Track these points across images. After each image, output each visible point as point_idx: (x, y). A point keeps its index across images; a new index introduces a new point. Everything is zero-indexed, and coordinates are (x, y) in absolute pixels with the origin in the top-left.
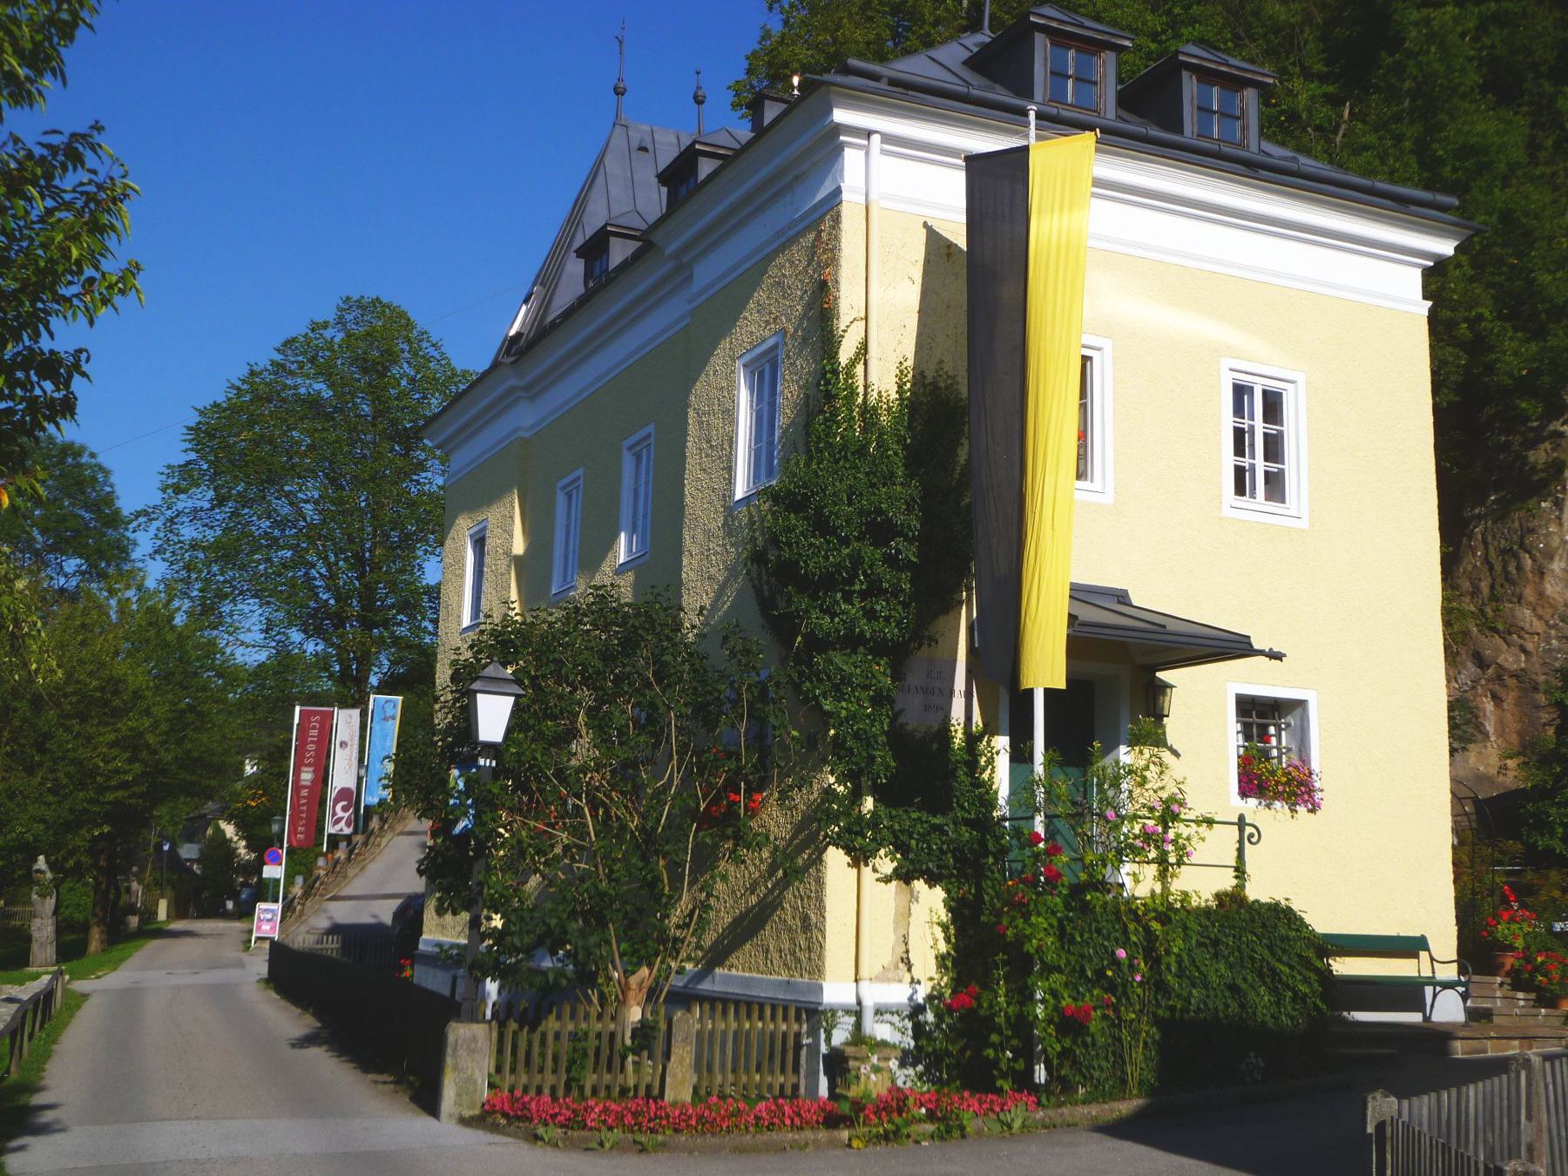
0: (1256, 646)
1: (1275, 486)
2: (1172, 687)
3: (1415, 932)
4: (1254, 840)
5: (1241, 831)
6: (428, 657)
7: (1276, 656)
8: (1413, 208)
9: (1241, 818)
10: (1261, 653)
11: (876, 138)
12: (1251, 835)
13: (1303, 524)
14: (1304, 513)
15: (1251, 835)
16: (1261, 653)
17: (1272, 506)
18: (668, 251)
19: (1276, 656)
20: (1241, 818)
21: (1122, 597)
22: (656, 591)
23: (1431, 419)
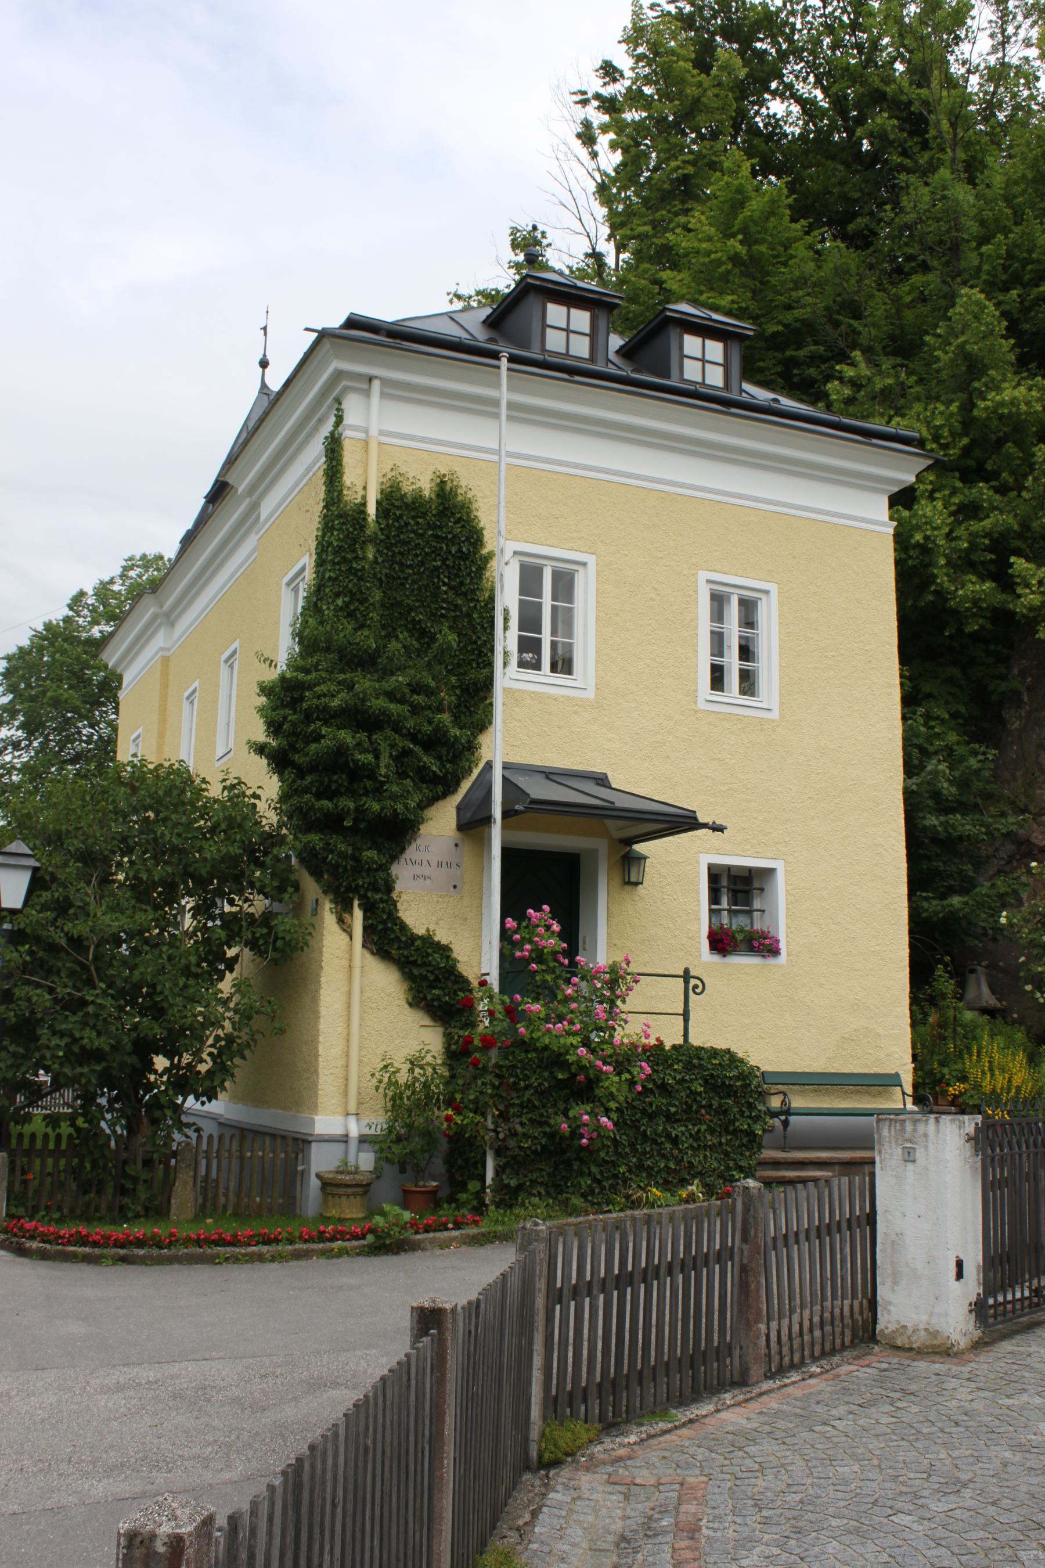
0: (702, 819)
1: (748, 682)
2: (645, 858)
3: (890, 1070)
4: (698, 990)
5: (686, 983)
6: (316, 873)
7: (719, 829)
8: (733, 410)
9: (687, 971)
10: (704, 826)
11: (376, 384)
12: (696, 986)
13: (775, 715)
14: (775, 705)
15: (696, 986)
16: (704, 826)
17: (560, 679)
18: (240, 490)
19: (719, 829)
20: (687, 971)
21: (602, 780)
22: (259, 792)
23: (894, 624)
